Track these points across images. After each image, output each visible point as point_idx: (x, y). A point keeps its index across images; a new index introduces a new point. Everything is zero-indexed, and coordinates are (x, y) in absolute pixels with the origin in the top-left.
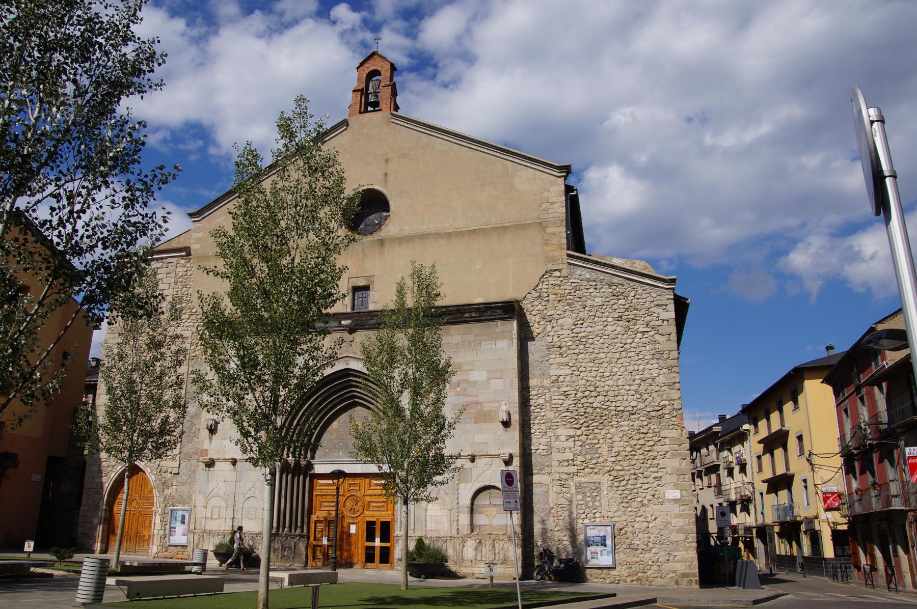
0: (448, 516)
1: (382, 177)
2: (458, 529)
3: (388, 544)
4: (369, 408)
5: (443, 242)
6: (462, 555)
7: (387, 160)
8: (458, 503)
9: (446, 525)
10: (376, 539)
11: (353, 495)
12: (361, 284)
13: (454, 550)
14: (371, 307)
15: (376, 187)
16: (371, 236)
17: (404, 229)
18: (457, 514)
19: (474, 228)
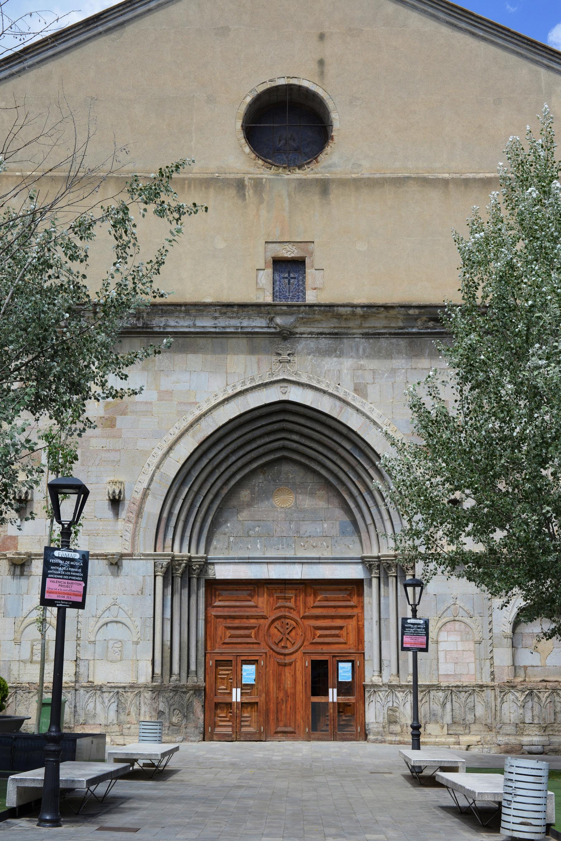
0: (474, 651)
1: (314, 66)
2: (492, 673)
3: (351, 699)
4: (315, 472)
5: (435, 195)
6: (501, 716)
7: (322, 37)
8: (490, 631)
9: (472, 666)
10: (330, 690)
11: (285, 617)
12: (289, 255)
13: (487, 707)
14: (311, 297)
15: (305, 84)
16: (300, 171)
17: (360, 165)
18: (491, 648)
19: (488, 175)
